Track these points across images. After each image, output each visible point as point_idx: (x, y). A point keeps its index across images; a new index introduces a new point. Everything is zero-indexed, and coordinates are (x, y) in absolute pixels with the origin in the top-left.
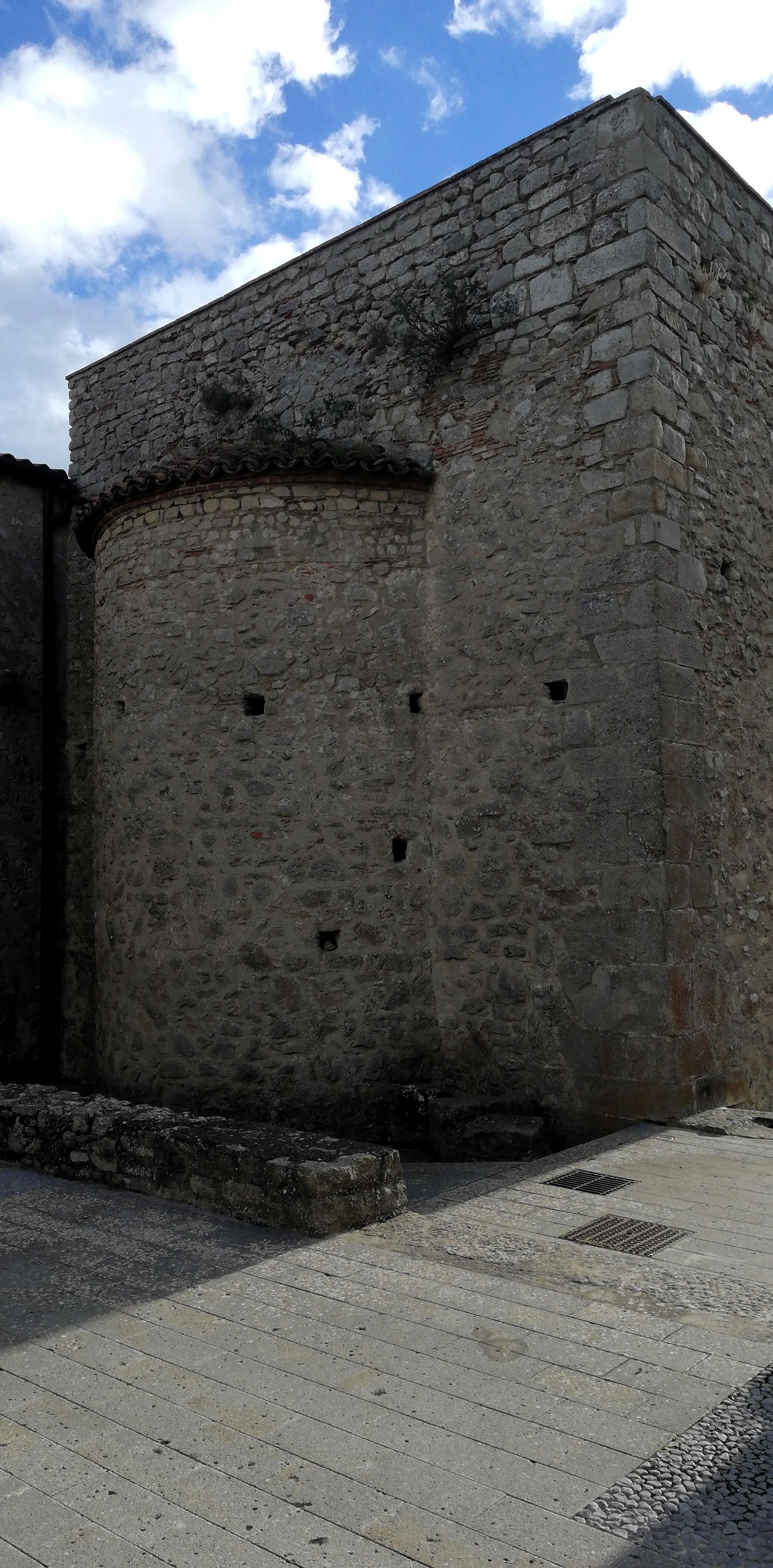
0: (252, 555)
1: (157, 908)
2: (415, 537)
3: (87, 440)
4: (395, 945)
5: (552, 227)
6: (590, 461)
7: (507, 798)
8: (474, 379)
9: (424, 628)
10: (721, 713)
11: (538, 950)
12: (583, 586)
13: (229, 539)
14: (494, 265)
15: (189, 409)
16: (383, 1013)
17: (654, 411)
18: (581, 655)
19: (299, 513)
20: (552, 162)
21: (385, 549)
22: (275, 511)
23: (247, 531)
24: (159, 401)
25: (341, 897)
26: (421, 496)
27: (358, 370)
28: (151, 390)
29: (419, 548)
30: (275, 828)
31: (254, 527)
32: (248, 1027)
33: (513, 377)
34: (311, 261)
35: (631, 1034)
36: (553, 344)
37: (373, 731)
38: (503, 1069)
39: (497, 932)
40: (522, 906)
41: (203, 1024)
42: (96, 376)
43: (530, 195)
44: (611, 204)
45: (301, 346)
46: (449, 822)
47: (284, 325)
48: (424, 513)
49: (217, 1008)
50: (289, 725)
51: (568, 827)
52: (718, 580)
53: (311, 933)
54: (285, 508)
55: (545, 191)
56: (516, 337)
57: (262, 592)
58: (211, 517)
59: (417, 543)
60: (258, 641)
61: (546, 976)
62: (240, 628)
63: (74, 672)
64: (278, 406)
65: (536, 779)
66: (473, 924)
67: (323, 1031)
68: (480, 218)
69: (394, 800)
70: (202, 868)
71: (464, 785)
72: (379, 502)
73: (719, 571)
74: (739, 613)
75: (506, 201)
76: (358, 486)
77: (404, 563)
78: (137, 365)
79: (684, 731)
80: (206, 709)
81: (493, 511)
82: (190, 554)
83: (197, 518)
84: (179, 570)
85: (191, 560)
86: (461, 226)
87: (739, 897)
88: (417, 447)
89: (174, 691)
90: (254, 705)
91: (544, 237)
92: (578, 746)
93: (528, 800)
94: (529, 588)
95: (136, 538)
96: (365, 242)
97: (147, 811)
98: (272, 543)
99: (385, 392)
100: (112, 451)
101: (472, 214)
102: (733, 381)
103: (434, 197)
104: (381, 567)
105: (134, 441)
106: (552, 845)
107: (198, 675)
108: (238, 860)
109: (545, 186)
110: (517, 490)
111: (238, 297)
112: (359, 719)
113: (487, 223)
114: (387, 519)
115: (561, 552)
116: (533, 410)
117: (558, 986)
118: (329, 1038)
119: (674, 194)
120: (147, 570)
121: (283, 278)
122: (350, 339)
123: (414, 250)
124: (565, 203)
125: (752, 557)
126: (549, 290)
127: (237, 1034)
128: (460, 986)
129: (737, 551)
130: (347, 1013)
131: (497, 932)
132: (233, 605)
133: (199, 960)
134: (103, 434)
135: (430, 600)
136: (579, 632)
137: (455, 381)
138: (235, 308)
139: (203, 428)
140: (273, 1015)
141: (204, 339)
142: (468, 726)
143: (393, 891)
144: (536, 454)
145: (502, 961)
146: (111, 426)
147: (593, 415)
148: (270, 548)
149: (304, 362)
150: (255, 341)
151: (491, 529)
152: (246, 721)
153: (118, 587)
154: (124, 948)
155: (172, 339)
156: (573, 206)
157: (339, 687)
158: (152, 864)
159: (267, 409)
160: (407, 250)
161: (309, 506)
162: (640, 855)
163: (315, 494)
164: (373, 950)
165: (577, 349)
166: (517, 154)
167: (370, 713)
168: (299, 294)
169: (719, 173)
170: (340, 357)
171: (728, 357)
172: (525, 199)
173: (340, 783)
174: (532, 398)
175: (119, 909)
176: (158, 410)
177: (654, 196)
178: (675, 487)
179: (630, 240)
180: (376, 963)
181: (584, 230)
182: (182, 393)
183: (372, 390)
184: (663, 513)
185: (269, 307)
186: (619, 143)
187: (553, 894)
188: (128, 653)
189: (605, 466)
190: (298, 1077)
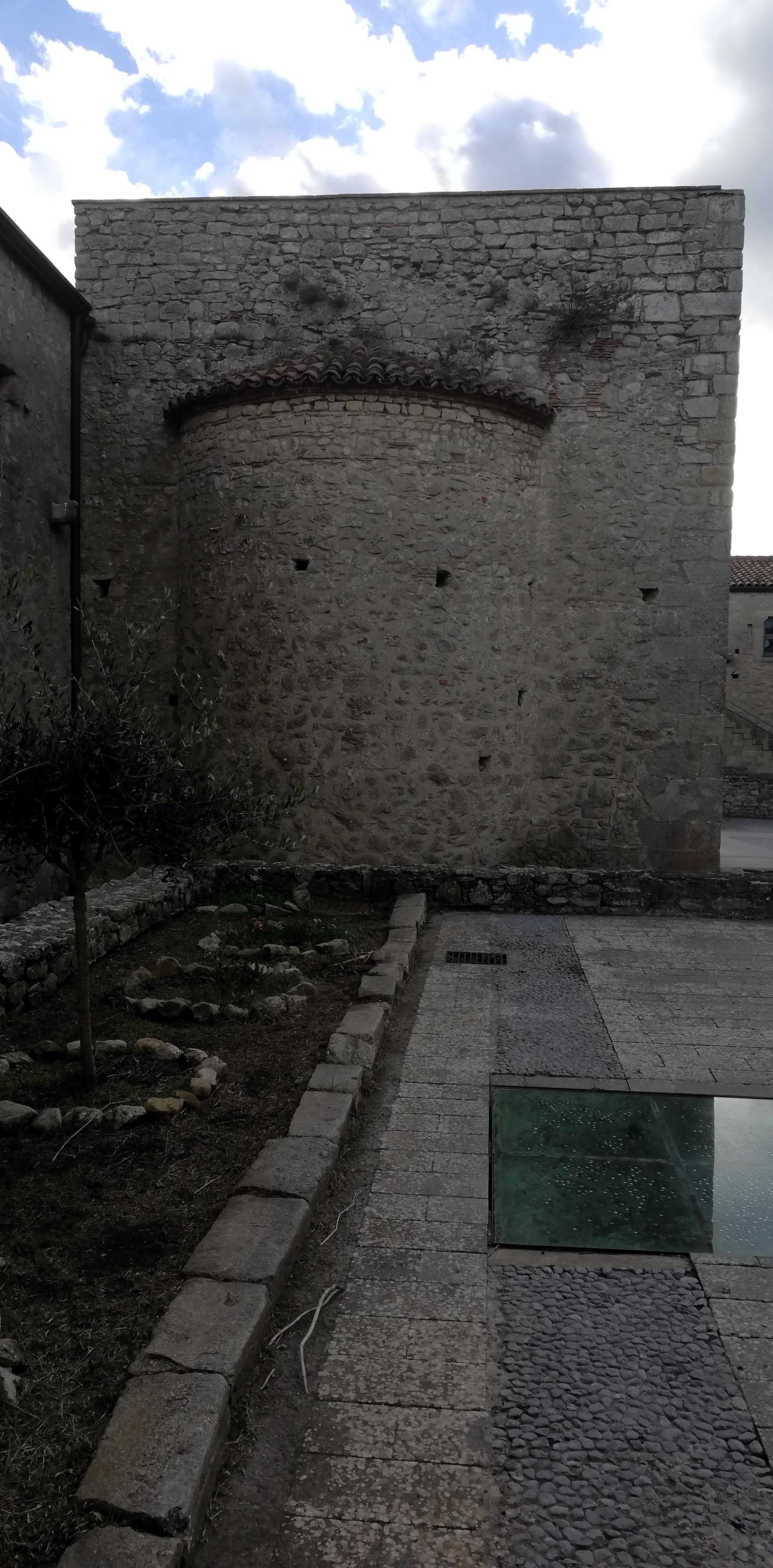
0: (449, 458)
1: (353, 739)
5: (667, 262)
6: (687, 441)
7: (603, 666)
8: (590, 355)
12: (677, 526)
16: (511, 816)
19: (483, 432)
20: (669, 214)
22: (467, 426)
23: (444, 437)
28: (206, 253)
30: (456, 678)
31: (451, 434)
32: (433, 826)
33: (625, 362)
36: (660, 348)
39: (591, 759)
40: (611, 741)
41: (396, 826)
43: (648, 232)
44: (716, 264)
46: (552, 681)
47: (389, 247)
48: (542, 445)
50: (468, 599)
51: (654, 689)
55: (663, 233)
58: (414, 419)
62: (436, 516)
63: (93, 507)
70: (398, 706)
71: (566, 654)
75: (627, 228)
76: (515, 417)
78: (185, 222)
80: (406, 578)
81: (603, 458)
82: (393, 446)
84: (383, 458)
85: (394, 452)
86: (583, 231)
89: (374, 559)
91: (660, 267)
92: (666, 635)
93: (622, 669)
94: (631, 519)
97: (341, 656)
100: (148, 298)
103: (560, 198)
106: (641, 700)
108: (428, 701)
109: (662, 229)
112: (507, 599)
115: (660, 499)
116: (642, 392)
117: (638, 794)
120: (347, 451)
121: (389, 204)
122: (463, 284)
124: (678, 249)
126: (662, 308)
127: (423, 833)
128: (553, 796)
131: (591, 759)
132: (432, 496)
140: (449, 818)
145: (589, 779)
146: (144, 272)
147: (692, 409)
148: (462, 455)
149: (410, 286)
150: (350, 249)
152: (437, 592)
157: (499, 573)
159: (364, 315)
160: (529, 230)
161: (488, 427)
168: (407, 225)
176: (216, 275)
181: (694, 274)
185: (369, 225)
187: (639, 733)
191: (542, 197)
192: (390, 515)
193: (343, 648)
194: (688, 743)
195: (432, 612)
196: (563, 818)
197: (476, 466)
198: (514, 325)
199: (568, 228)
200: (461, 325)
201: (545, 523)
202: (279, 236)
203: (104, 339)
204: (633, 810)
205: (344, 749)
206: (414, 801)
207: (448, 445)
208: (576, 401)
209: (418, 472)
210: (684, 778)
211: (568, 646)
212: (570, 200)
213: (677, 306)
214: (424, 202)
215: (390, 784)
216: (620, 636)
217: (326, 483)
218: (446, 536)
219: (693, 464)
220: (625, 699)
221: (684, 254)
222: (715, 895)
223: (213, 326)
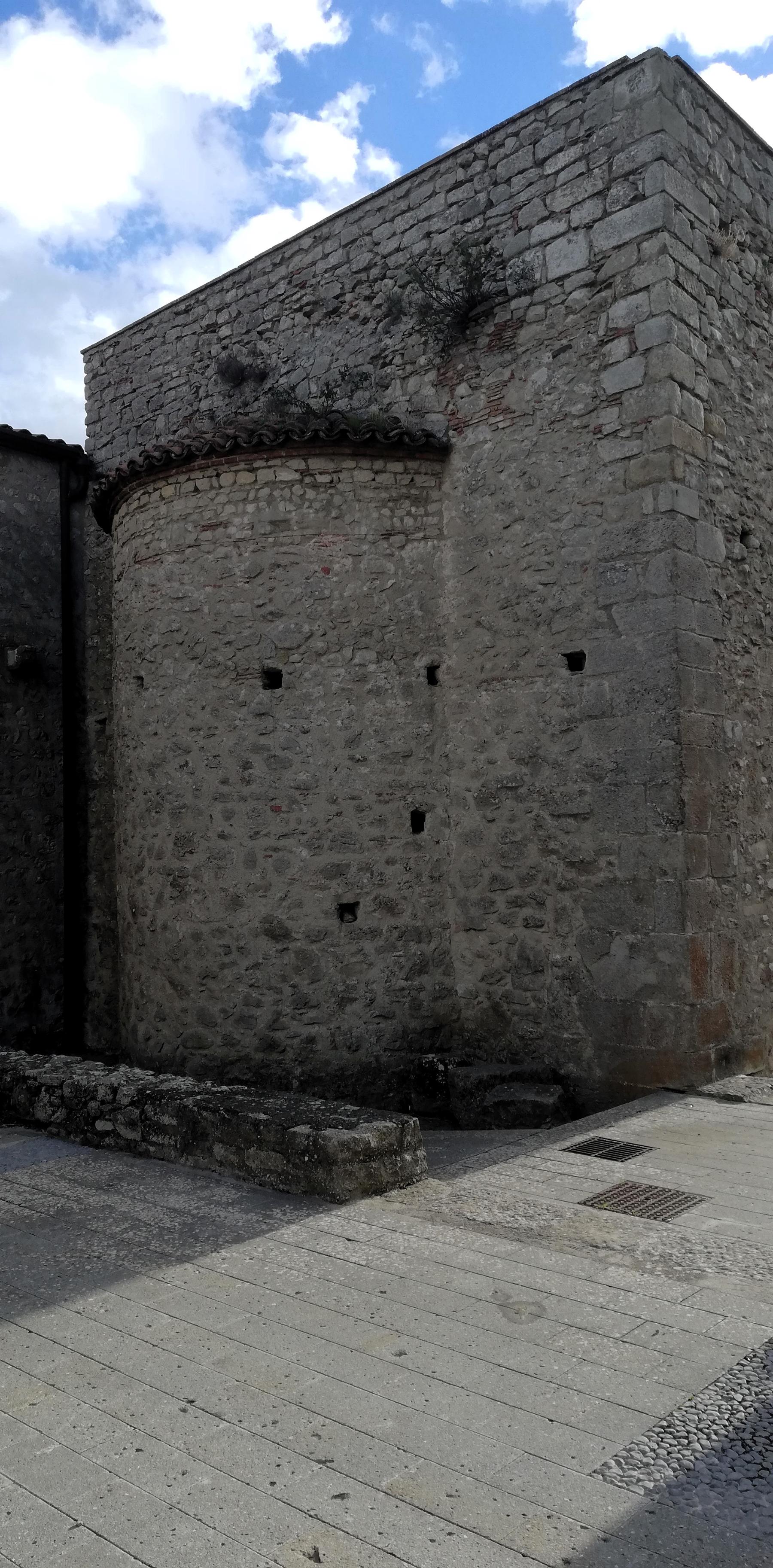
0: (269, 528)
1: (178, 882)
2: (432, 508)
3: (103, 415)
5: (568, 192)
6: (607, 430)
7: (525, 770)
9: (441, 600)
10: (740, 682)
11: (557, 921)
12: (601, 556)
13: (245, 513)
14: (510, 232)
15: (204, 382)
16: (403, 983)
17: (671, 378)
18: (599, 625)
19: (315, 486)
20: (567, 125)
21: (402, 520)
22: (290, 484)
23: (263, 504)
24: (174, 375)
25: (360, 870)
26: (437, 467)
27: (373, 340)
28: (166, 363)
29: (435, 520)
30: (294, 801)
31: (270, 500)
32: (269, 998)
33: (529, 345)
35: (650, 1003)
36: (570, 311)
37: (390, 703)
38: (522, 1038)
39: (516, 903)
40: (540, 877)
44: (628, 168)
45: (316, 316)
46: (468, 795)
48: (441, 483)
49: (239, 979)
50: (307, 698)
52: (738, 548)
53: (330, 905)
54: (301, 481)
57: (279, 566)
59: (433, 514)
60: (276, 615)
61: (564, 946)
62: (256, 602)
64: (294, 378)
65: (554, 750)
67: (344, 1001)
68: (495, 184)
69: (413, 772)
70: (222, 842)
71: (482, 757)
72: (395, 474)
73: (738, 539)
74: (759, 582)
75: (522, 167)
77: (421, 535)
78: (152, 338)
80: (224, 683)
81: (510, 482)
82: (206, 528)
83: (213, 492)
84: (196, 545)
85: (208, 535)
86: (476, 193)
87: (758, 866)
89: (193, 666)
90: (273, 679)
91: (560, 202)
92: (596, 717)
93: (546, 771)
94: (546, 558)
95: (153, 512)
96: (379, 210)
97: (167, 785)
98: (288, 516)
100: (128, 426)
101: (487, 180)
102: (753, 345)
103: (449, 163)
104: (398, 539)
105: (150, 415)
106: (570, 816)
107: (215, 650)
108: (257, 833)
109: (561, 150)
110: (534, 459)
112: (377, 692)
113: (502, 188)
114: (404, 490)
116: (550, 379)
117: (576, 957)
118: (349, 1008)
119: (692, 155)
120: (164, 545)
121: (296, 248)
122: (365, 309)
124: (581, 167)
126: (565, 256)
127: (258, 1005)
128: (479, 956)
129: (757, 519)
131: (516, 903)
132: (249, 580)
133: (220, 932)
134: (119, 408)
135: (447, 572)
136: (596, 602)
137: (471, 350)
138: (249, 279)
139: (218, 402)
140: (294, 986)
141: (219, 311)
142: (485, 698)
144: (552, 422)
145: (520, 931)
146: (127, 400)
147: (610, 383)
148: (286, 521)
149: (319, 333)
150: (269, 312)
151: (508, 500)
152: (264, 695)
153: (136, 562)
155: (187, 311)
156: (589, 170)
157: (356, 661)
158: (173, 837)
159: (282, 381)
163: (331, 466)
165: (594, 316)
166: (532, 118)
167: (388, 686)
168: (314, 263)
170: (355, 327)
172: (540, 163)
173: (358, 756)
174: (548, 366)
176: (173, 384)
177: (671, 158)
178: (693, 455)
179: (647, 203)
180: (396, 934)
181: (601, 194)
182: (197, 366)
184: (681, 481)
185: (283, 278)
187: (572, 864)
188: (146, 628)
189: (623, 434)
194: (635, 879)
195: (257, 721)
198: (410, 341)
199: (461, 197)
201: (450, 584)
206: (245, 963)
207: (268, 513)
209: (234, 553)
210: (633, 932)
212: (459, 160)
215: (215, 941)
216: (542, 725)
218: (273, 625)
219: (617, 461)
220: (553, 815)
222: (249, 1143)
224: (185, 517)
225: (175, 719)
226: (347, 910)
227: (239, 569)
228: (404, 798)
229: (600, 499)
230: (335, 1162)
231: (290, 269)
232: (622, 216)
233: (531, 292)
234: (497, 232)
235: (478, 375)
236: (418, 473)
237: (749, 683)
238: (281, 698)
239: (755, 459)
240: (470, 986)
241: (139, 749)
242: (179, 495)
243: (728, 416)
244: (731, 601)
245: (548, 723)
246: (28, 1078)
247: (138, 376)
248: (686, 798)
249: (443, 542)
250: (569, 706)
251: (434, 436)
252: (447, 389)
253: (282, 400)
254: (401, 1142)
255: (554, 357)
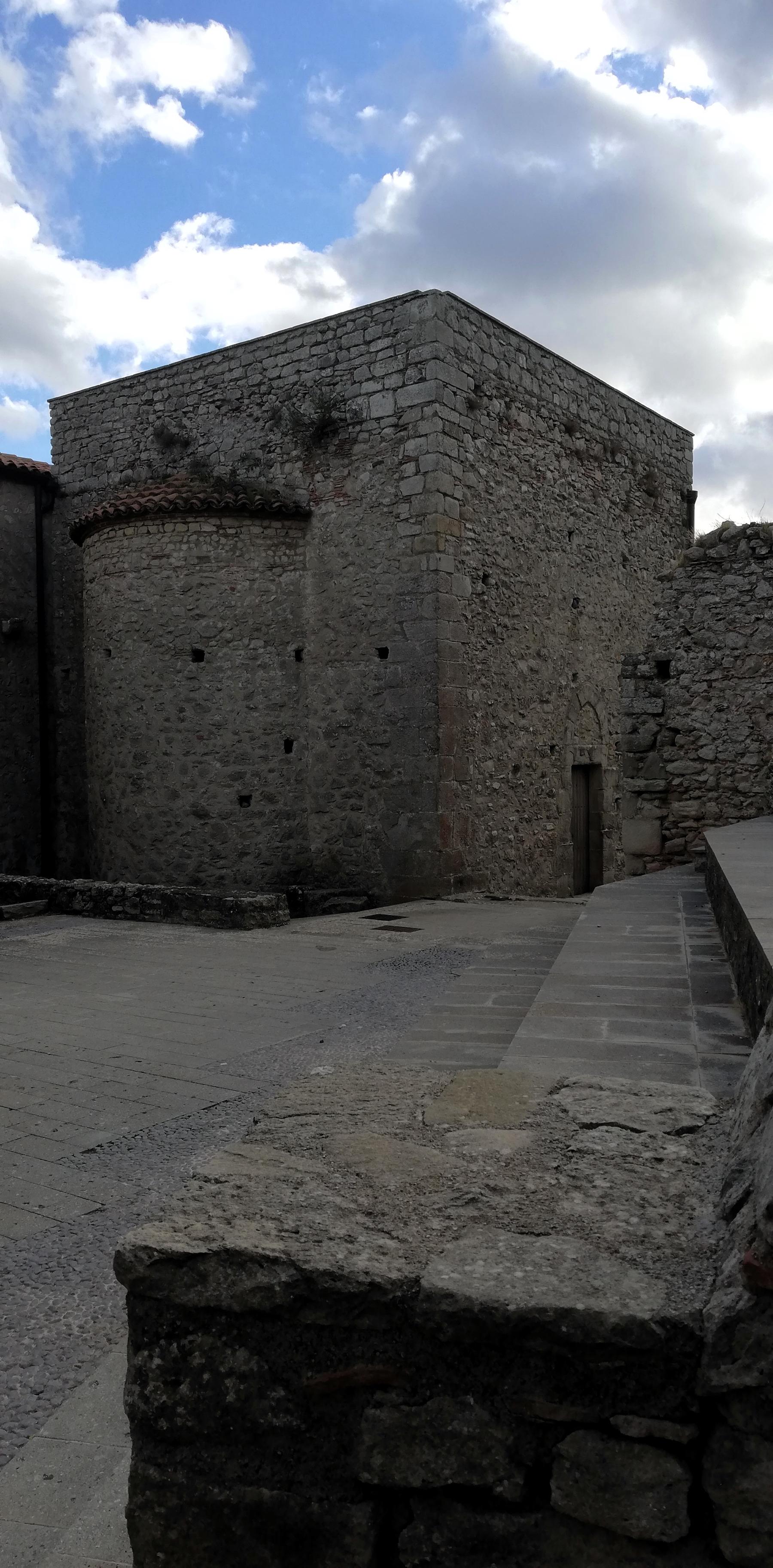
0: (196, 561)
1: (136, 783)
2: (300, 550)
3: (65, 450)
4: (285, 804)
5: (383, 365)
6: (402, 517)
8: (336, 454)
9: (304, 609)
10: (479, 667)
11: (369, 806)
13: (180, 550)
14: (349, 382)
15: (144, 439)
16: (279, 844)
17: (438, 491)
18: (395, 633)
19: (226, 536)
20: (384, 323)
21: (280, 558)
22: (210, 534)
23: (192, 545)
24: (121, 430)
25: (252, 775)
26: (303, 525)
27: (263, 434)
28: (115, 421)
29: (301, 558)
30: (212, 733)
34: (231, 353)
35: (418, 851)
36: (383, 439)
37: (272, 673)
38: (348, 874)
39: (347, 796)
42: (72, 404)
43: (370, 342)
44: (417, 359)
45: (224, 409)
46: (320, 730)
47: (212, 393)
48: (305, 535)
49: (177, 842)
50: (220, 669)
52: (480, 587)
53: (234, 797)
54: (217, 532)
55: (379, 341)
56: (361, 431)
57: (202, 585)
58: (169, 534)
59: (300, 555)
60: (201, 616)
61: (373, 821)
62: (188, 607)
63: (59, 618)
64: (209, 449)
65: (370, 706)
66: (332, 791)
67: (243, 854)
68: (340, 348)
69: (285, 716)
71: (329, 707)
72: (276, 529)
73: (480, 581)
74: (494, 605)
75: (357, 342)
77: (292, 567)
78: (104, 401)
79: (453, 680)
80: (167, 657)
82: (155, 558)
83: (160, 535)
84: (148, 568)
85: (156, 562)
86: (329, 351)
87: (487, 775)
88: (300, 491)
89: (146, 645)
90: (198, 656)
91: (378, 370)
92: (393, 687)
94: (367, 590)
95: (118, 544)
96: (267, 347)
98: (209, 554)
99: (280, 452)
100: (86, 461)
101: (336, 345)
102: (495, 459)
104: (278, 570)
105: (102, 456)
107: (161, 636)
109: (379, 338)
110: (361, 528)
111: (179, 367)
112: (264, 667)
113: (344, 353)
114: (282, 539)
116: (371, 480)
117: (380, 826)
118: (245, 859)
119: (456, 351)
120: (126, 566)
121: (210, 360)
122: (257, 412)
123: (299, 361)
124: (390, 352)
125: (504, 569)
126: (381, 405)
127: (189, 857)
128: (324, 828)
129: (494, 567)
130: (256, 845)
131: (347, 796)
132: (184, 592)
133: (163, 813)
134: (78, 447)
135: (308, 591)
136: (395, 619)
137: (324, 453)
138: (177, 374)
139: (154, 455)
141: (154, 391)
142: (331, 672)
143: (284, 773)
144: (372, 507)
146: (85, 442)
147: (405, 488)
150: (192, 400)
151: (345, 551)
152: (193, 666)
153: (105, 574)
154: (114, 807)
155: (131, 387)
156: (395, 355)
157: (251, 646)
158: (133, 754)
159: (200, 449)
160: (294, 359)
161: (231, 531)
162: (425, 751)
163: (236, 524)
164: (272, 808)
165: (397, 445)
166: (363, 313)
167: (271, 662)
168: (223, 373)
169: (489, 326)
170: (250, 422)
171: (492, 443)
172: (368, 343)
173: (252, 706)
174: (370, 471)
175: (110, 782)
176: (120, 437)
177: (442, 357)
178: (451, 535)
179: (427, 384)
180: (274, 814)
181: (402, 371)
182: (138, 427)
183: (272, 449)
184: (444, 552)
185: (201, 378)
186: (422, 322)
187: (378, 773)
188: (114, 619)
189: (412, 521)
190: (226, 882)
191: (285, 337)
192: (155, 611)
193: (129, 715)
196: (331, 847)
197: (222, 564)
200: (254, 446)
202: (153, 400)
203: (64, 496)
204: (376, 840)
205: (132, 792)
206: (180, 832)
207: (195, 552)
208: (328, 495)
209: (174, 575)
211: (329, 701)
213: (392, 401)
214: (231, 353)
216: (363, 690)
217: (116, 591)
221: (395, 355)
222: (201, 908)
223: (119, 475)
224: (141, 550)
225: (134, 679)
226: (244, 800)
227: (177, 584)
228: (280, 732)
229: (398, 558)
230: (246, 912)
231: (206, 373)
232: (413, 388)
233: (361, 423)
234: (341, 380)
235: (328, 470)
236: (290, 528)
237: (485, 667)
238: (203, 669)
239: (494, 530)
240: (319, 846)
241: (108, 697)
242: (137, 535)
243: (475, 507)
244: (475, 619)
245: (367, 689)
246: (68, 888)
247: (93, 427)
248: (440, 735)
249: (306, 572)
250: (379, 679)
251: (301, 507)
252: (309, 475)
253: (200, 468)
254: (277, 905)
255: (374, 467)
